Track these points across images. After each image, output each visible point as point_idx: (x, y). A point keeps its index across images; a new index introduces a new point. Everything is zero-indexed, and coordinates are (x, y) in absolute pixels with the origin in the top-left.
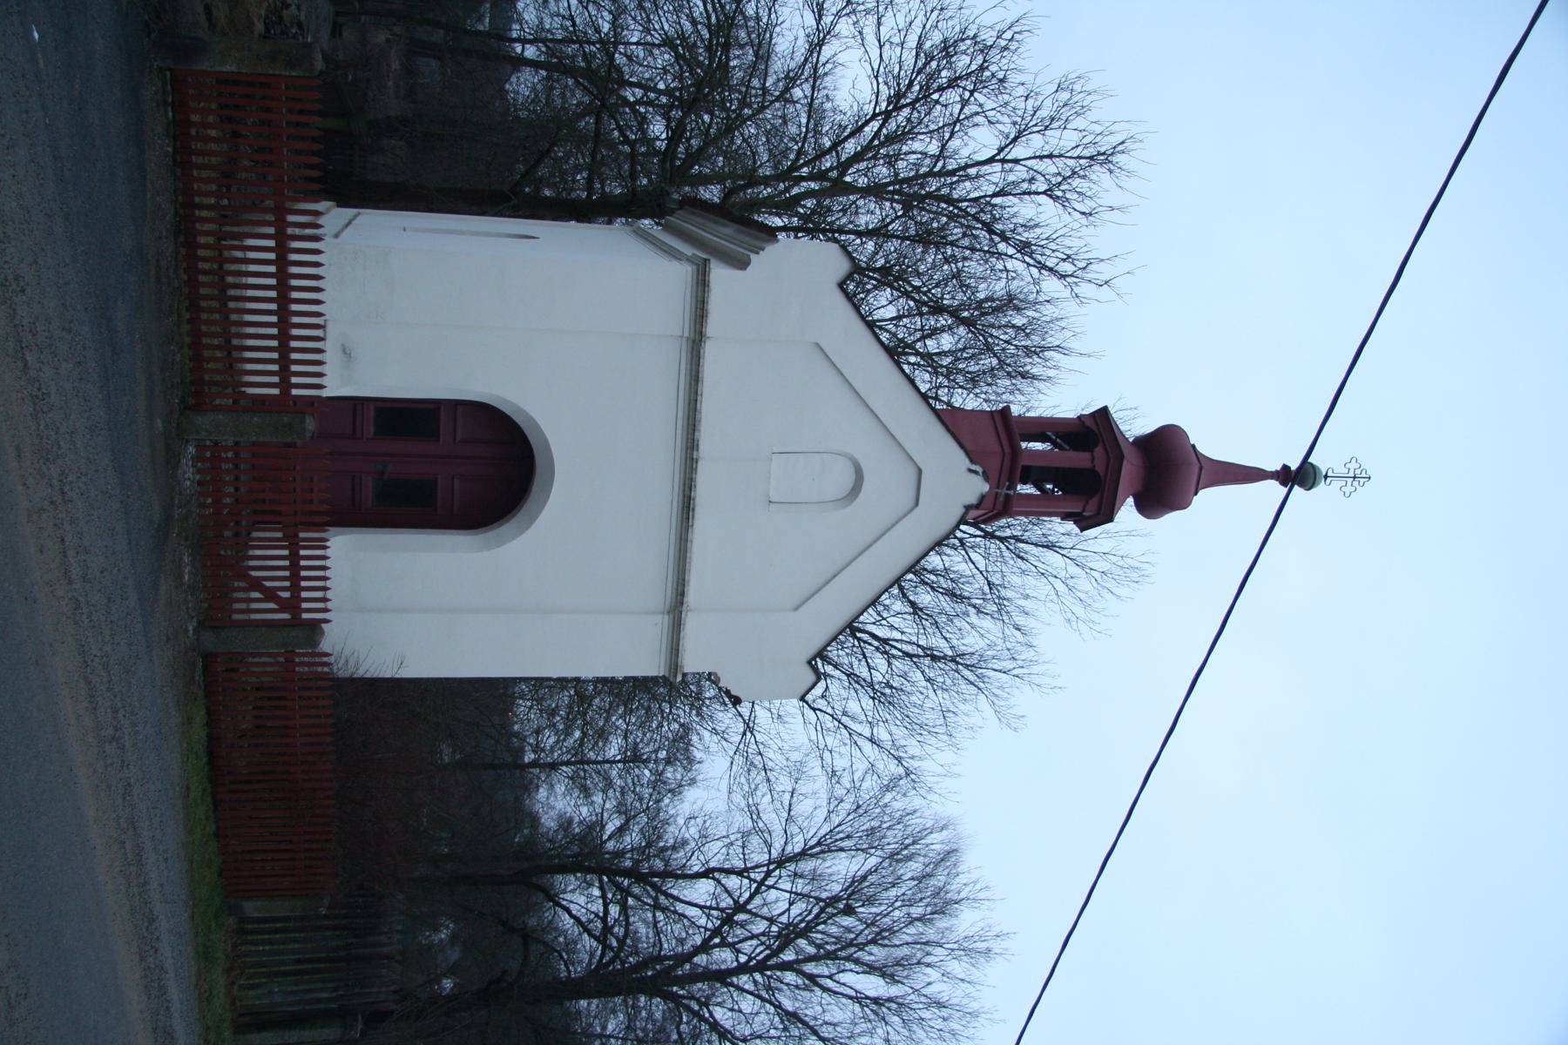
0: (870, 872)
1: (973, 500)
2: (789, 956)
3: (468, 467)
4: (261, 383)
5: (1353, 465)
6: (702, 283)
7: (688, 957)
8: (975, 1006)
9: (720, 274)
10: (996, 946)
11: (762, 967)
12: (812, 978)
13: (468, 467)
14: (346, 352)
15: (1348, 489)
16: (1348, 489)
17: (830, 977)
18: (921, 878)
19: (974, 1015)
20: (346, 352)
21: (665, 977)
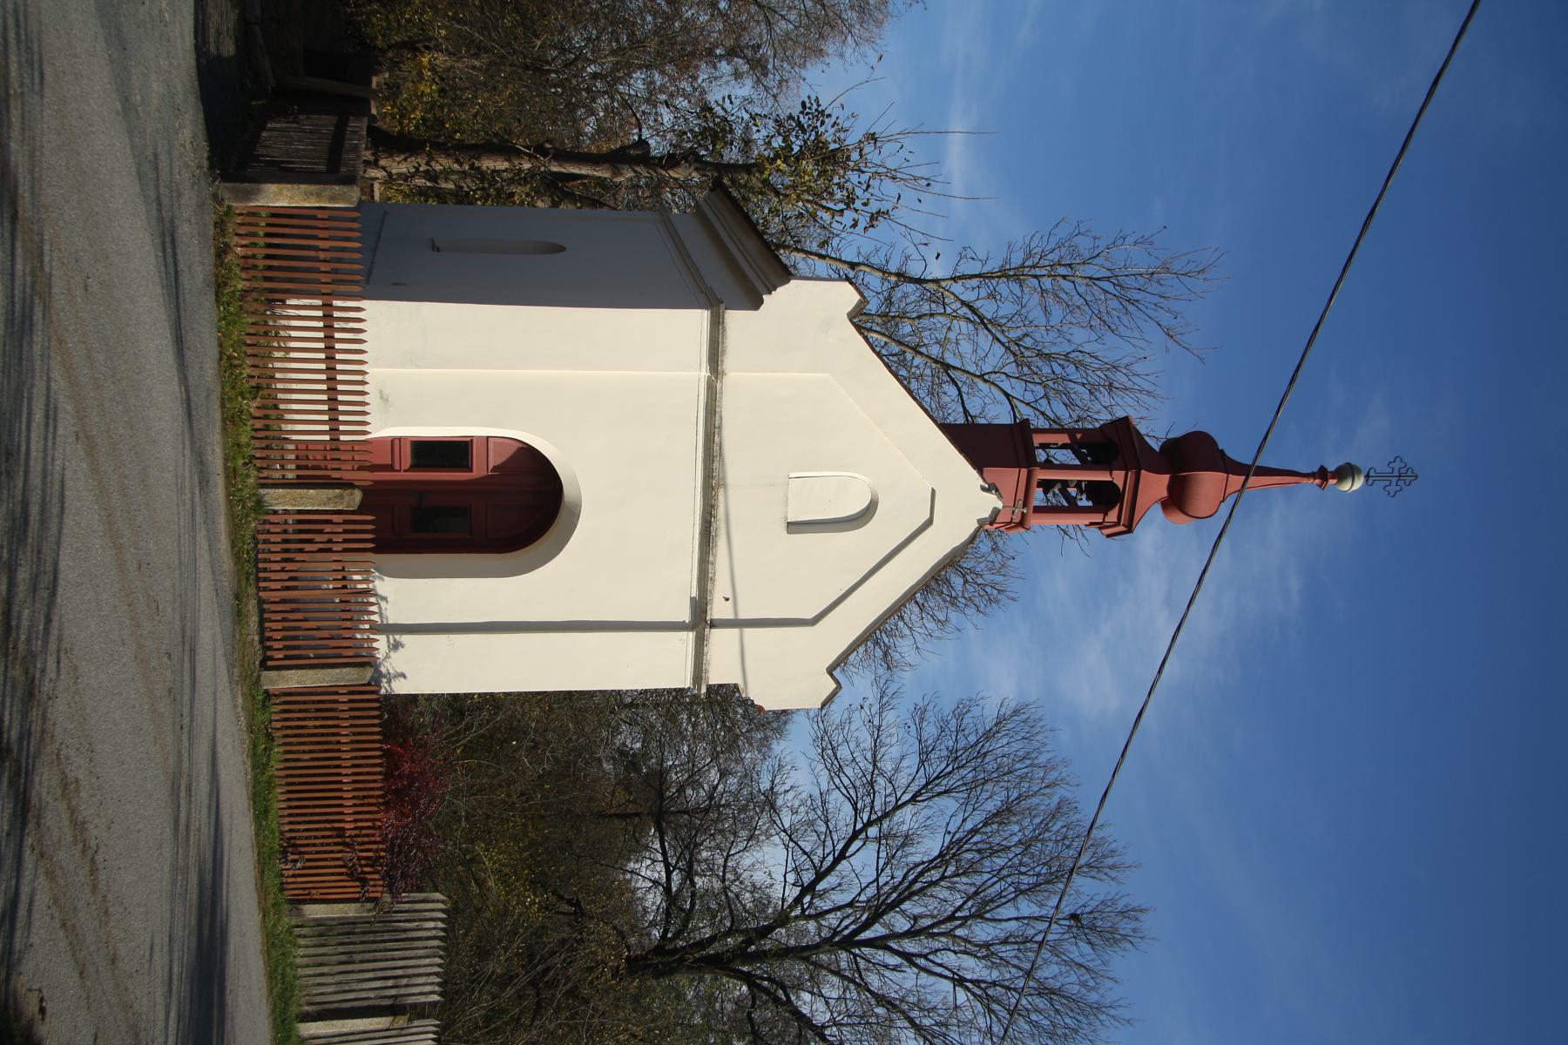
0: (974, 831)
1: (986, 514)
2: (877, 930)
3: (500, 505)
4: (305, 424)
5: (1397, 465)
6: (717, 325)
7: (765, 932)
8: (1093, 997)
9: (736, 319)
10: (1125, 926)
11: (849, 943)
12: (908, 957)
13: (500, 505)
14: (383, 398)
15: (1392, 489)
16: (1392, 489)
17: (925, 957)
18: (1026, 844)
19: (1097, 1008)
20: (383, 398)
21: (752, 948)
